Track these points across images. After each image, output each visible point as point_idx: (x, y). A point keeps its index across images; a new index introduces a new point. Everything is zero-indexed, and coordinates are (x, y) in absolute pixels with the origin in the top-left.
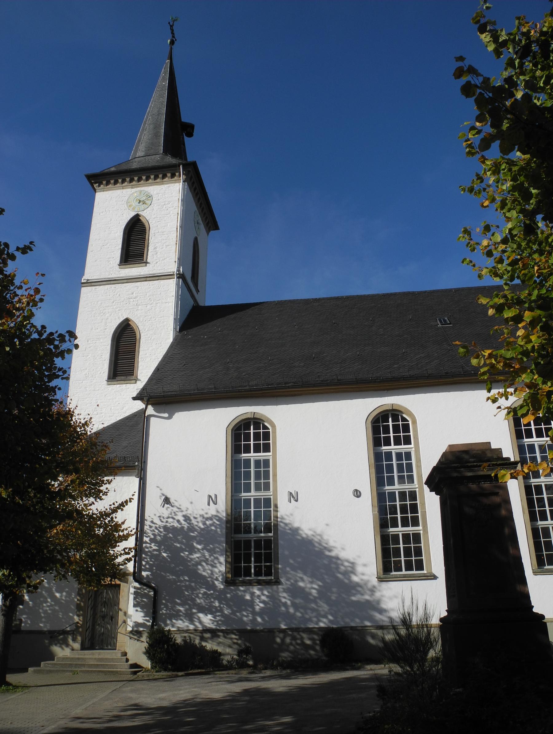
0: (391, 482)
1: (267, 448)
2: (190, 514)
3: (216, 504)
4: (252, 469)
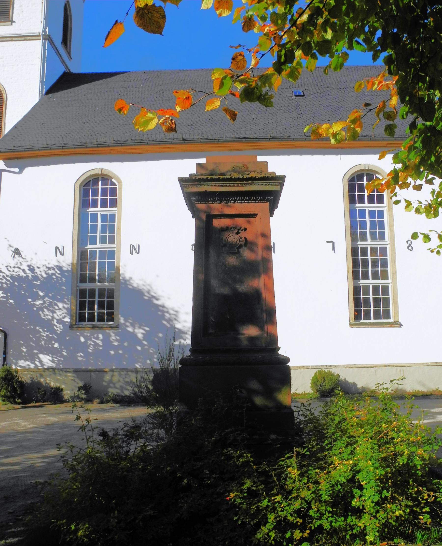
0: (364, 238)
1: (113, 203)
2: (34, 265)
3: (63, 255)
4: (99, 223)
